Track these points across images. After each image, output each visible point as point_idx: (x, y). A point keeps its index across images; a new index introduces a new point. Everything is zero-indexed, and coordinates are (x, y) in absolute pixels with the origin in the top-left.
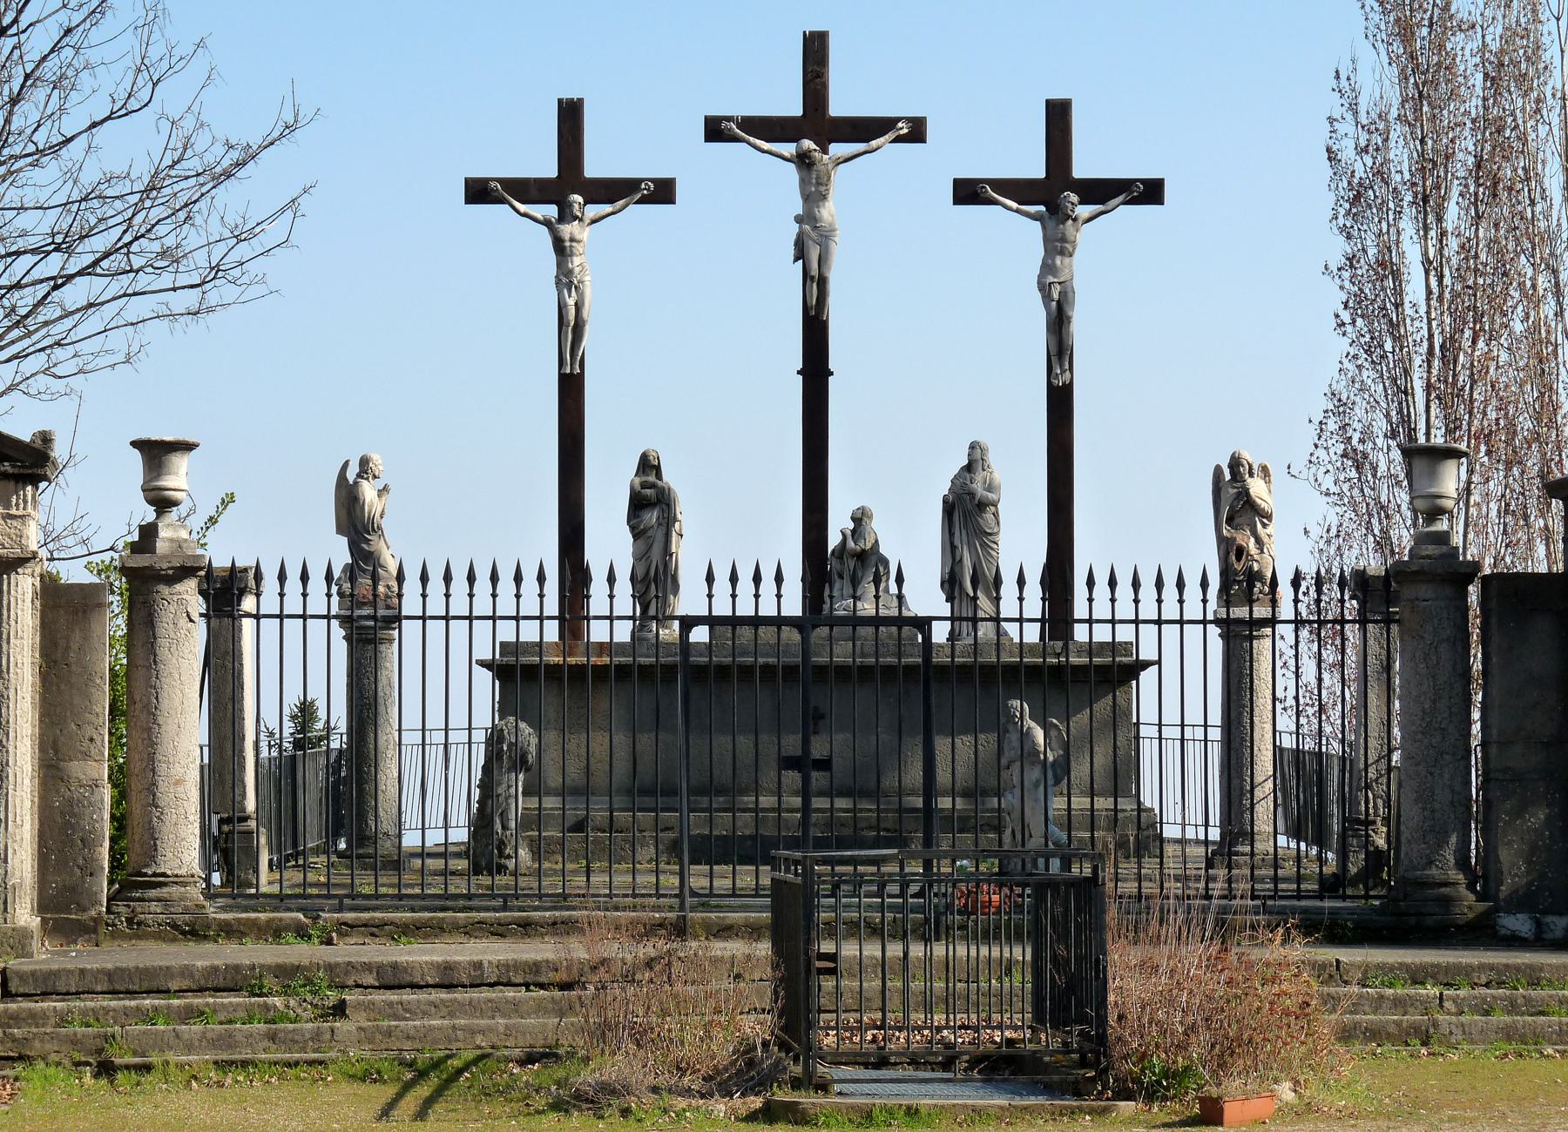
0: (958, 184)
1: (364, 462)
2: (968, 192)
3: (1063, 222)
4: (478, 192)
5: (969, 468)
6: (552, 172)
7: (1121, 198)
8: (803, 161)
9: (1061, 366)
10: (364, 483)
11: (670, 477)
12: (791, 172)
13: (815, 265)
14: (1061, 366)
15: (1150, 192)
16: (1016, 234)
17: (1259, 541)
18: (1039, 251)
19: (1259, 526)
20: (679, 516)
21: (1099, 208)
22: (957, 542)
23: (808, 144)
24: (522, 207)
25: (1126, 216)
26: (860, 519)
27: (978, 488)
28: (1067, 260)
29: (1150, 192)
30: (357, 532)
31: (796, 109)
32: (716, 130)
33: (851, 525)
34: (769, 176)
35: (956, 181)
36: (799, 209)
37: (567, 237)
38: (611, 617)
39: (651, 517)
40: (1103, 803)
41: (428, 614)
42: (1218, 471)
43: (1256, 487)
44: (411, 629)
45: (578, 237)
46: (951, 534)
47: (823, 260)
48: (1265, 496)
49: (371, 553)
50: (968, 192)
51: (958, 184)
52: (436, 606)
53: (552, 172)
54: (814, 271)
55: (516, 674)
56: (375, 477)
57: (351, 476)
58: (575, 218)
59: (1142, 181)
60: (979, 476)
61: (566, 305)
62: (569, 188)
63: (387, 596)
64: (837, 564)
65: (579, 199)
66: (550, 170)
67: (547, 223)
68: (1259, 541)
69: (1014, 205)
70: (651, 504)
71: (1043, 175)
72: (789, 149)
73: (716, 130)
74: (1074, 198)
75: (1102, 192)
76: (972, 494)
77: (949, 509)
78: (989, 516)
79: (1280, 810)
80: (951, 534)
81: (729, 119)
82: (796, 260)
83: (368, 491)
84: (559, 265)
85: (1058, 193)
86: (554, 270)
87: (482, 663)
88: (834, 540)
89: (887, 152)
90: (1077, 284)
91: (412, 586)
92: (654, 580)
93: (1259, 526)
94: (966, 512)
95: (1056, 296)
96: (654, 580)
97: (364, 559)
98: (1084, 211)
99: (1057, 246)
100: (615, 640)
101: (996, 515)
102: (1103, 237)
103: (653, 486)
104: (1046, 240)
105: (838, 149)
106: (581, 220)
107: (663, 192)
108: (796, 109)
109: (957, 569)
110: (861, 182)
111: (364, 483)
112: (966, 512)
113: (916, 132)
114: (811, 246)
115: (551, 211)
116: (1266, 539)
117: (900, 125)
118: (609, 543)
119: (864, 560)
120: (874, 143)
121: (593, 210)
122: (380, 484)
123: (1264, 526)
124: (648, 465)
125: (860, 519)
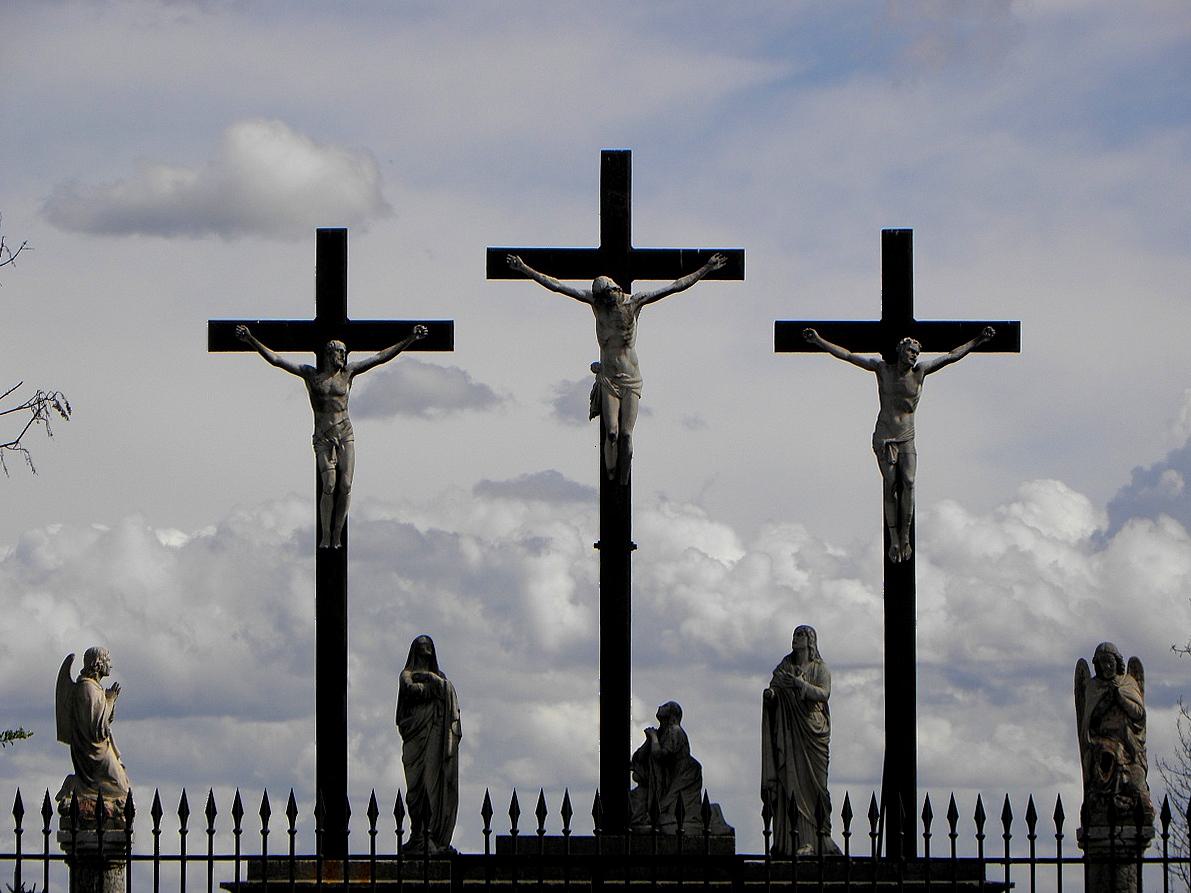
0: (781, 327)
1: (91, 656)
2: (792, 337)
3: (903, 374)
5: (793, 658)
6: (876, 315)
7: (969, 344)
8: (601, 301)
9: (901, 538)
12: (585, 317)
13: (615, 421)
14: (901, 538)
15: (1004, 337)
16: (849, 388)
17: (1129, 749)
21: (945, 355)
22: (780, 744)
23: (607, 281)
24: (270, 352)
25: (976, 364)
26: (670, 714)
27: (659, 757)
28: (907, 417)
29: (1004, 337)
30: (81, 738)
31: (594, 242)
32: (501, 264)
33: (657, 725)
34: (560, 327)
35: (778, 324)
36: (596, 356)
37: (327, 389)
39: (424, 713)
41: (162, 853)
42: (1082, 664)
43: (1126, 684)
44: (142, 870)
45: (340, 389)
46: (774, 736)
47: (625, 416)
48: (1137, 696)
49: (98, 763)
50: (792, 337)
51: (781, 327)
52: (170, 844)
53: (876, 315)
54: (615, 430)
57: (75, 673)
58: (337, 367)
59: (994, 324)
60: (805, 668)
61: (326, 469)
63: (115, 812)
64: (647, 774)
65: (341, 345)
66: (307, 311)
67: (304, 372)
68: (1129, 749)
69: (846, 352)
70: (426, 706)
71: (877, 317)
72: (584, 285)
73: (501, 264)
74: (915, 344)
75: (950, 337)
76: (797, 688)
77: (770, 703)
78: (818, 715)
79: (787, 818)
80: (774, 736)
83: (96, 690)
84: (317, 422)
85: (896, 340)
86: (311, 428)
87: (224, 885)
88: (637, 740)
89: (706, 291)
91: (142, 824)
92: (431, 795)
94: (792, 708)
95: (894, 459)
96: (431, 795)
97: (89, 771)
98: (926, 358)
99: (897, 401)
101: (826, 712)
102: (368, 382)
105: (641, 287)
106: (343, 370)
107: (439, 336)
108: (594, 242)
110: (671, 328)
111: (91, 682)
112: (792, 708)
113: (731, 265)
114: (611, 395)
115: (309, 359)
117: (713, 259)
119: (671, 757)
120: (683, 280)
121: (356, 357)
123: (95, 754)
124: (422, 654)
125: (670, 714)
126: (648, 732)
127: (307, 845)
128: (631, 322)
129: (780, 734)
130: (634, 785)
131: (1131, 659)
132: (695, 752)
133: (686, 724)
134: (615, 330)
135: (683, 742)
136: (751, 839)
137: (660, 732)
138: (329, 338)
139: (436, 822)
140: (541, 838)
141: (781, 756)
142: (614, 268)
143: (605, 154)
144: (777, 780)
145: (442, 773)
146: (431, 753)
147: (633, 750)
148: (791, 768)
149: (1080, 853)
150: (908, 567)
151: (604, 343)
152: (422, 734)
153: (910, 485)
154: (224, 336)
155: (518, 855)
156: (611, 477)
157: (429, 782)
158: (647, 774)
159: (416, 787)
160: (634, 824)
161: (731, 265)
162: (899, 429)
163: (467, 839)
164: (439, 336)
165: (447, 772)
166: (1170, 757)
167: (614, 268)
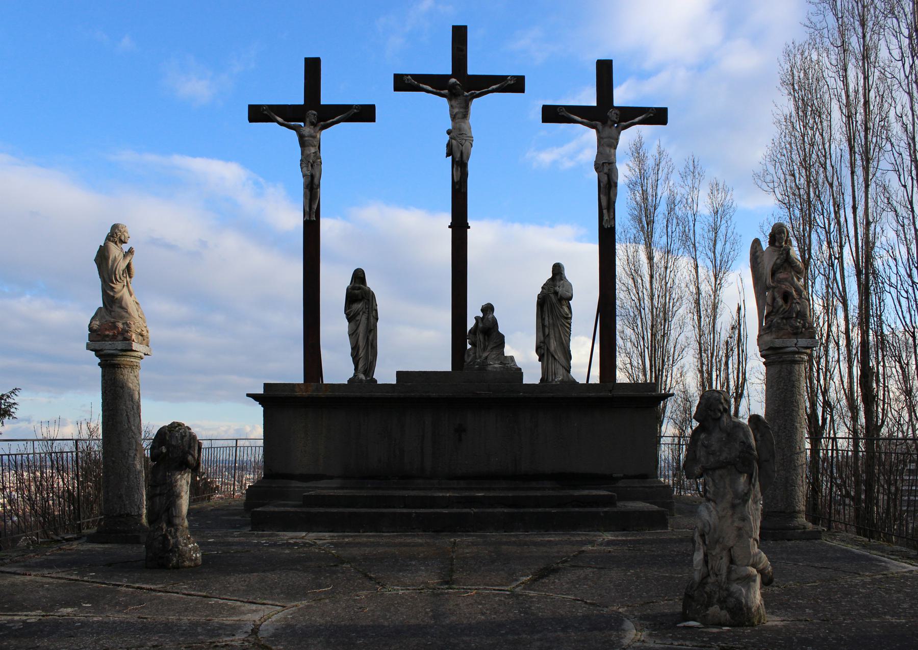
2: (552, 114)
5: (553, 279)
10: (112, 245)
11: (371, 283)
22: (546, 323)
26: (488, 309)
27: (560, 290)
33: (481, 315)
34: (437, 108)
36: (449, 125)
38: (338, 367)
39: (357, 306)
40: (912, 498)
55: (273, 399)
62: (310, 114)
64: (476, 337)
70: (360, 298)
81: (407, 75)
82: (448, 155)
86: (300, 157)
88: (471, 324)
92: (364, 347)
96: (364, 347)
102: (335, 139)
103: (359, 288)
112: (553, 302)
118: (335, 327)
119: (489, 331)
122: (126, 248)
124: (359, 277)
125: (488, 309)
127: (595, 378)
129: (547, 318)
130: (469, 346)
131: (175, 427)
132: (501, 330)
133: (496, 314)
134: (460, 115)
135: (495, 323)
136: (532, 374)
137: (483, 319)
139: (904, 318)
142: (460, 86)
143: (454, 27)
144: (544, 342)
145: (368, 339)
146: (362, 329)
147: (469, 329)
148: (552, 336)
149: (385, 374)
150: (612, 230)
151: (453, 117)
154: (258, 114)
156: (457, 187)
157: (361, 343)
159: (849, 404)
160: (728, 578)
161: (516, 85)
162: (609, 156)
163: (385, 374)
165: (370, 338)
167: (460, 86)
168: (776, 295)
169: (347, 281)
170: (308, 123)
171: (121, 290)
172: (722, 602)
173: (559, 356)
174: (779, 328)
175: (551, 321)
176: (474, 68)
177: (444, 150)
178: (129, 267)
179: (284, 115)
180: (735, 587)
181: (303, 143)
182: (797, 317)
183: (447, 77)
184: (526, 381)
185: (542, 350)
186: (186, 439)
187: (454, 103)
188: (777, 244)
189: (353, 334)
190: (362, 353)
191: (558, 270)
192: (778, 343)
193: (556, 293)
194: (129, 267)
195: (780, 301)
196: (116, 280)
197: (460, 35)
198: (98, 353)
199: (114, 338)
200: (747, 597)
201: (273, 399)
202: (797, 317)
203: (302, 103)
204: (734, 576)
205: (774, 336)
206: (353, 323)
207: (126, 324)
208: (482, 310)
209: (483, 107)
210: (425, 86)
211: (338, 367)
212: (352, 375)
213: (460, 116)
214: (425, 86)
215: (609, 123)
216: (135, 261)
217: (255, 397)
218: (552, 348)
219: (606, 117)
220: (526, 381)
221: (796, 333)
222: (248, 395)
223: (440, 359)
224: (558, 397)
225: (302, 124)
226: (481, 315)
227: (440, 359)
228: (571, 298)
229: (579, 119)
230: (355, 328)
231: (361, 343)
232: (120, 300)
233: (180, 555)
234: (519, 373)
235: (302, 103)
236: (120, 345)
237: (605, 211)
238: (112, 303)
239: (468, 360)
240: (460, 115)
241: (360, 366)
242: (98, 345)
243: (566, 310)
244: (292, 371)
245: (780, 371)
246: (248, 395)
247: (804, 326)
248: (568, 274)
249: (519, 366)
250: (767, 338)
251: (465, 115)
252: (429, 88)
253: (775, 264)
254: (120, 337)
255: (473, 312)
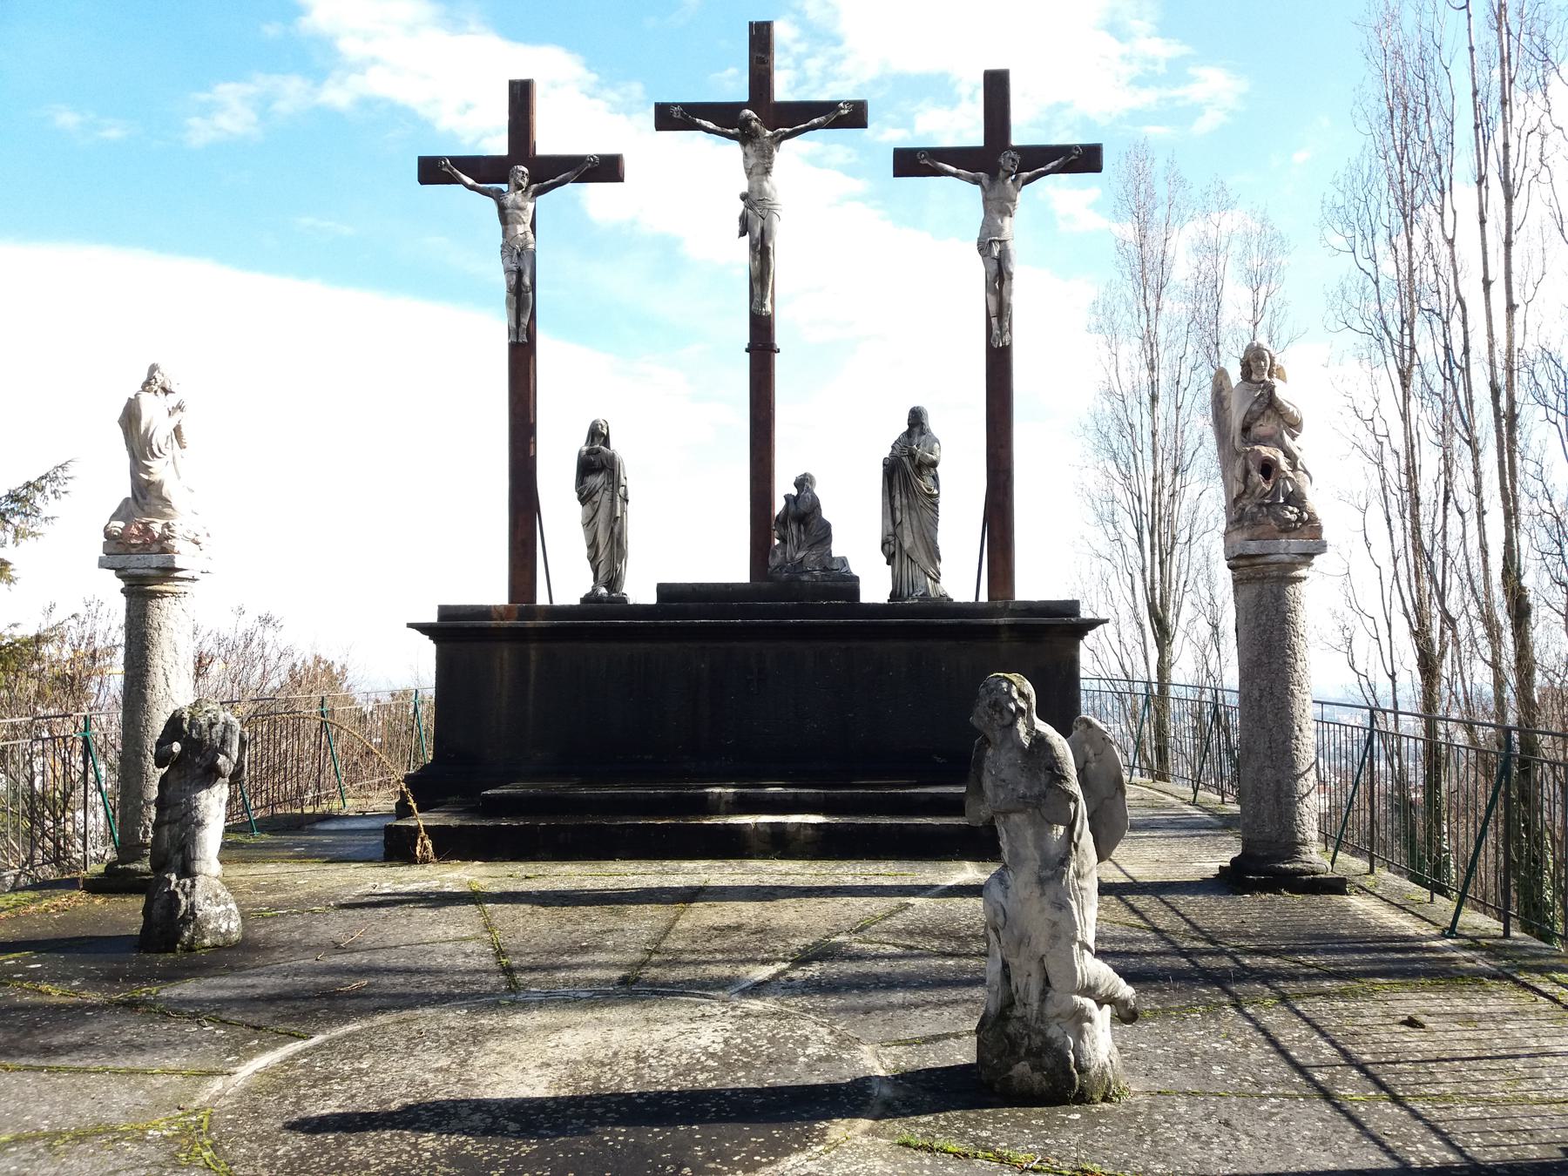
0: (862, 124)
2: (910, 163)
4: (433, 171)
11: (618, 446)
17: (1289, 455)
18: (979, 214)
19: (1287, 438)
20: (623, 481)
26: (803, 483)
33: (794, 492)
34: (717, 160)
39: (597, 480)
51: (862, 124)
56: (166, 391)
64: (786, 524)
70: (597, 467)
82: (742, 234)
85: (998, 162)
86: (500, 241)
88: (779, 505)
90: (1011, 245)
92: (607, 548)
93: (1287, 438)
96: (607, 548)
100: (556, 603)
101: (935, 478)
104: (986, 200)
107: (607, 169)
109: (757, 289)
112: (908, 474)
114: (756, 223)
116: (1297, 452)
119: (806, 516)
122: (172, 400)
123: (1293, 437)
124: (597, 434)
125: (803, 483)
126: (787, 497)
128: (771, 152)
132: (826, 515)
135: (815, 506)
136: (875, 587)
137: (796, 499)
138: (519, 169)
140: (604, 614)
141: (898, 514)
142: (761, 119)
144: (894, 535)
146: (602, 516)
148: (906, 524)
149: (639, 589)
151: (749, 173)
152: (596, 498)
153: (1010, 275)
155: (676, 598)
157: (602, 539)
158: (786, 524)
161: (853, 116)
164: (607, 169)
165: (616, 530)
166: (752, 975)
167: (761, 119)
168: (1251, 466)
169: (579, 442)
170: (513, 187)
171: (159, 469)
172: (1035, 1055)
173: (921, 556)
174: (1255, 522)
175: (905, 501)
176: (784, 90)
177: (736, 227)
178: (177, 431)
179: (720, 118)
180: (1053, 1032)
181: (506, 216)
182: (1287, 502)
183: (739, 106)
184: (865, 598)
185: (892, 549)
186: (218, 728)
187: (748, 148)
188: (1254, 377)
189: (589, 523)
190: (603, 555)
191: (917, 419)
192: (1253, 547)
193: (912, 455)
194: (177, 431)
195: (1257, 477)
196: (154, 455)
197: (996, 86)
198: (121, 572)
199: (145, 548)
200: (1078, 1051)
201: (454, 631)
202: (1287, 502)
203: (504, 152)
204: (1050, 1010)
205: (1246, 536)
206: (588, 506)
207: (167, 526)
208: (796, 485)
209: (796, 155)
210: (704, 122)
211: (566, 579)
212: (589, 590)
213: (760, 170)
214: (704, 122)
215: (1001, 174)
216: (187, 420)
217: (423, 628)
218: (907, 545)
219: (998, 162)
220: (865, 598)
221: (1287, 528)
222: (410, 625)
223: (729, 563)
224: (920, 621)
225: (504, 187)
226: (794, 492)
227: (729, 563)
228: (934, 464)
229: (953, 169)
230: (591, 514)
231: (602, 539)
232: (159, 486)
233: (197, 926)
234: (850, 585)
235: (504, 152)
236: (157, 561)
237: (994, 321)
238: (145, 496)
239: (773, 562)
240: (760, 167)
241: (601, 574)
242: (119, 561)
243: (929, 481)
244: (493, 591)
245: (1260, 596)
246: (410, 625)
247: (1300, 519)
248: (934, 424)
249: (855, 571)
250: (1238, 537)
251: (767, 171)
252: (711, 125)
253: (1249, 412)
254: (155, 548)
255: (783, 488)
